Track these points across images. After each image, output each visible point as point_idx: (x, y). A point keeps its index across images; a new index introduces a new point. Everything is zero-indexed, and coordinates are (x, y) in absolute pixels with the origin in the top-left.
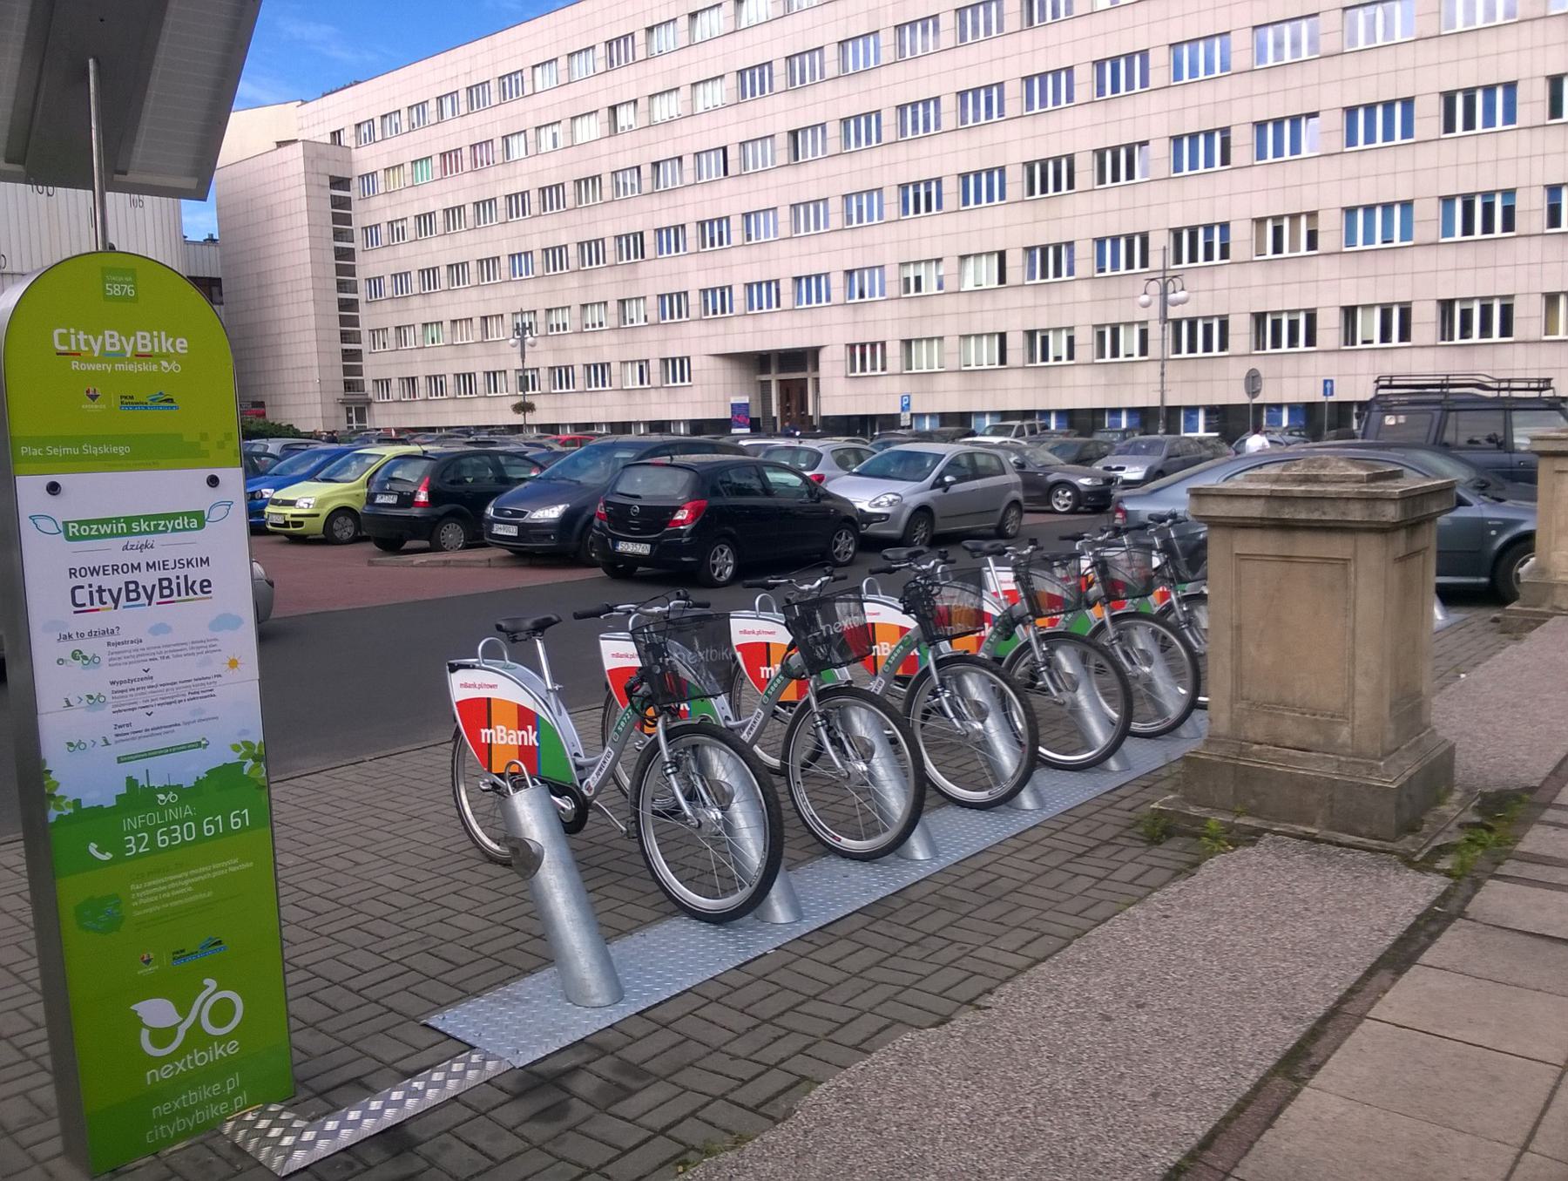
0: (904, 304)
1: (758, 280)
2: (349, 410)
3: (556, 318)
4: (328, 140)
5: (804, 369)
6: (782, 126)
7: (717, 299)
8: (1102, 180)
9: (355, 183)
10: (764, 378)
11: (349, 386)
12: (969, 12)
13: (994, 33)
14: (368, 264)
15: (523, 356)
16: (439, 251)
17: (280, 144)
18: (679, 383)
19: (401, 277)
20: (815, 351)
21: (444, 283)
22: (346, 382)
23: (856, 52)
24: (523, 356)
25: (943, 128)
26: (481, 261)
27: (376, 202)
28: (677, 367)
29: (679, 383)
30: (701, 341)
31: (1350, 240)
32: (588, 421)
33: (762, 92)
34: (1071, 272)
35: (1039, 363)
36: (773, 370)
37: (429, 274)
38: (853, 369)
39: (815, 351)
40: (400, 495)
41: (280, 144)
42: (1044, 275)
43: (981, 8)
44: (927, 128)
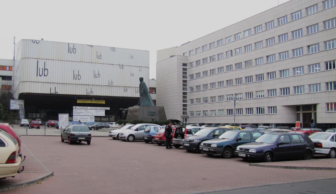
0: (281, 98)
1: (273, 88)
2: (183, 119)
3: (238, 96)
4: (182, 55)
5: (311, 110)
6: (265, 55)
7: (285, 91)
8: (327, 69)
9: (188, 65)
10: (298, 112)
11: (184, 113)
12: (310, 27)
13: (300, 36)
14: (191, 83)
15: (235, 105)
16: (208, 80)
17: (172, 56)
18: (250, 114)
19: (198, 87)
20: (315, 106)
21: (209, 88)
22: (183, 112)
23: (260, 45)
24: (235, 105)
25: (253, 66)
26: (203, 85)
27: (193, 69)
28: (273, 109)
29: (250, 114)
30: (280, 102)
31: (310, 91)
32: (219, 123)
33: (299, 36)
34: (289, 94)
35: (270, 114)
36: (301, 110)
37: (205, 86)
38: (328, 110)
39: (315, 106)
40: (38, 127)
41: (172, 56)
42: (284, 94)
43: (330, 21)
44: (286, 58)
